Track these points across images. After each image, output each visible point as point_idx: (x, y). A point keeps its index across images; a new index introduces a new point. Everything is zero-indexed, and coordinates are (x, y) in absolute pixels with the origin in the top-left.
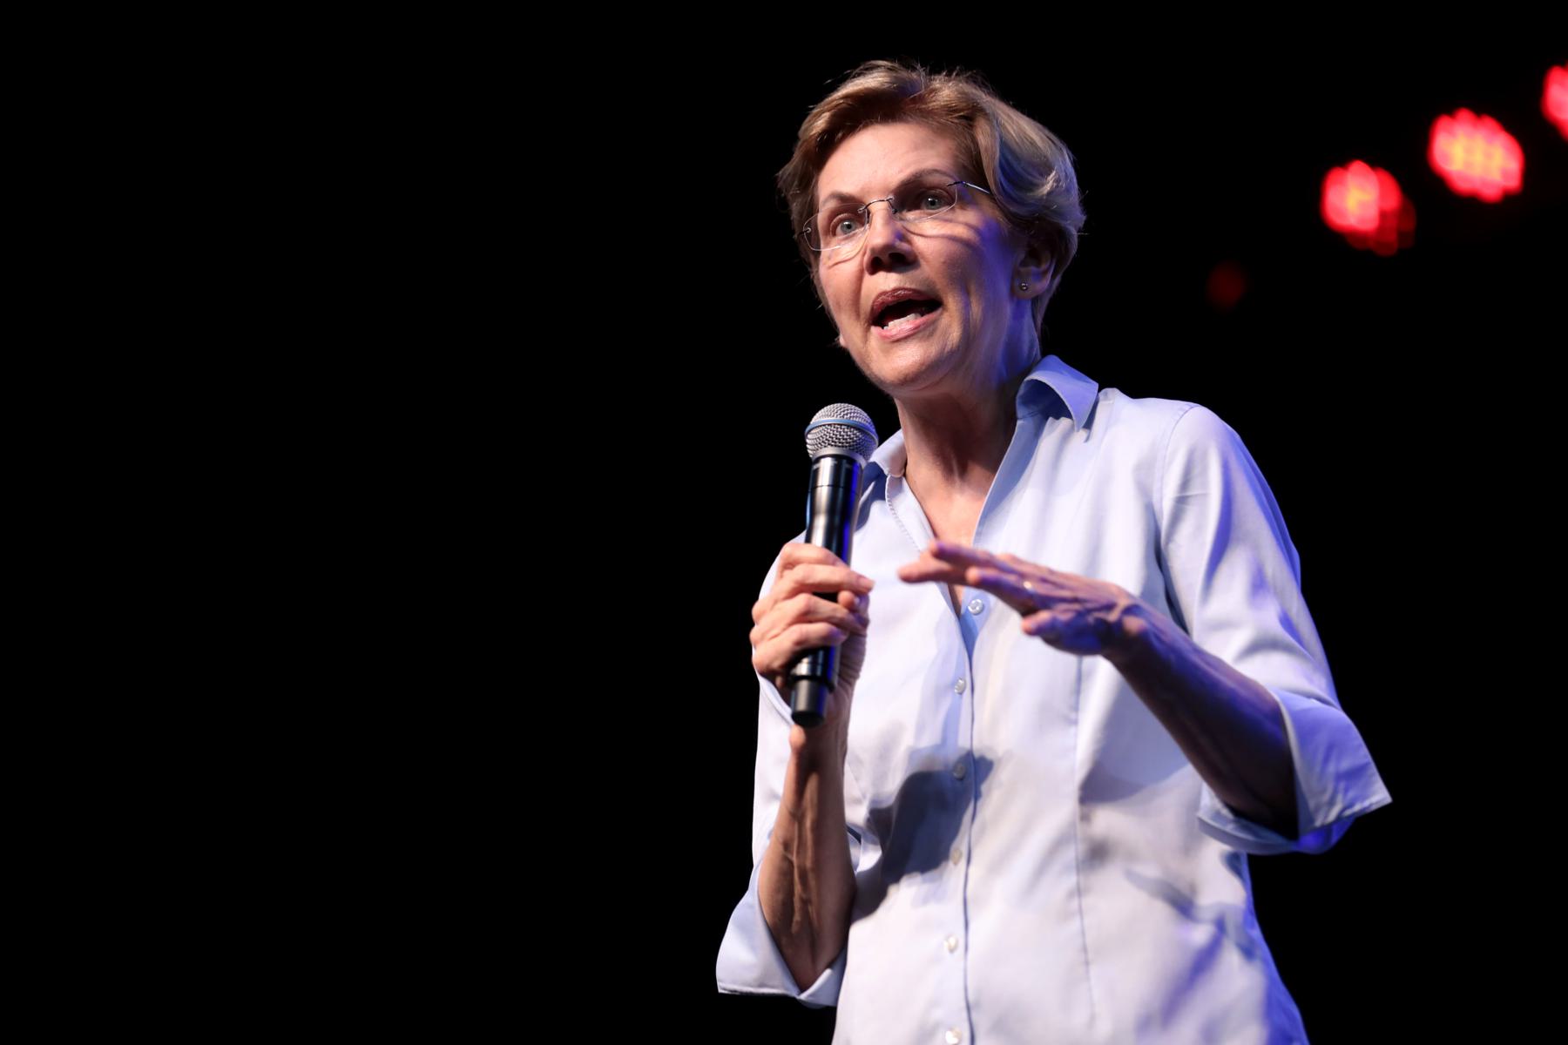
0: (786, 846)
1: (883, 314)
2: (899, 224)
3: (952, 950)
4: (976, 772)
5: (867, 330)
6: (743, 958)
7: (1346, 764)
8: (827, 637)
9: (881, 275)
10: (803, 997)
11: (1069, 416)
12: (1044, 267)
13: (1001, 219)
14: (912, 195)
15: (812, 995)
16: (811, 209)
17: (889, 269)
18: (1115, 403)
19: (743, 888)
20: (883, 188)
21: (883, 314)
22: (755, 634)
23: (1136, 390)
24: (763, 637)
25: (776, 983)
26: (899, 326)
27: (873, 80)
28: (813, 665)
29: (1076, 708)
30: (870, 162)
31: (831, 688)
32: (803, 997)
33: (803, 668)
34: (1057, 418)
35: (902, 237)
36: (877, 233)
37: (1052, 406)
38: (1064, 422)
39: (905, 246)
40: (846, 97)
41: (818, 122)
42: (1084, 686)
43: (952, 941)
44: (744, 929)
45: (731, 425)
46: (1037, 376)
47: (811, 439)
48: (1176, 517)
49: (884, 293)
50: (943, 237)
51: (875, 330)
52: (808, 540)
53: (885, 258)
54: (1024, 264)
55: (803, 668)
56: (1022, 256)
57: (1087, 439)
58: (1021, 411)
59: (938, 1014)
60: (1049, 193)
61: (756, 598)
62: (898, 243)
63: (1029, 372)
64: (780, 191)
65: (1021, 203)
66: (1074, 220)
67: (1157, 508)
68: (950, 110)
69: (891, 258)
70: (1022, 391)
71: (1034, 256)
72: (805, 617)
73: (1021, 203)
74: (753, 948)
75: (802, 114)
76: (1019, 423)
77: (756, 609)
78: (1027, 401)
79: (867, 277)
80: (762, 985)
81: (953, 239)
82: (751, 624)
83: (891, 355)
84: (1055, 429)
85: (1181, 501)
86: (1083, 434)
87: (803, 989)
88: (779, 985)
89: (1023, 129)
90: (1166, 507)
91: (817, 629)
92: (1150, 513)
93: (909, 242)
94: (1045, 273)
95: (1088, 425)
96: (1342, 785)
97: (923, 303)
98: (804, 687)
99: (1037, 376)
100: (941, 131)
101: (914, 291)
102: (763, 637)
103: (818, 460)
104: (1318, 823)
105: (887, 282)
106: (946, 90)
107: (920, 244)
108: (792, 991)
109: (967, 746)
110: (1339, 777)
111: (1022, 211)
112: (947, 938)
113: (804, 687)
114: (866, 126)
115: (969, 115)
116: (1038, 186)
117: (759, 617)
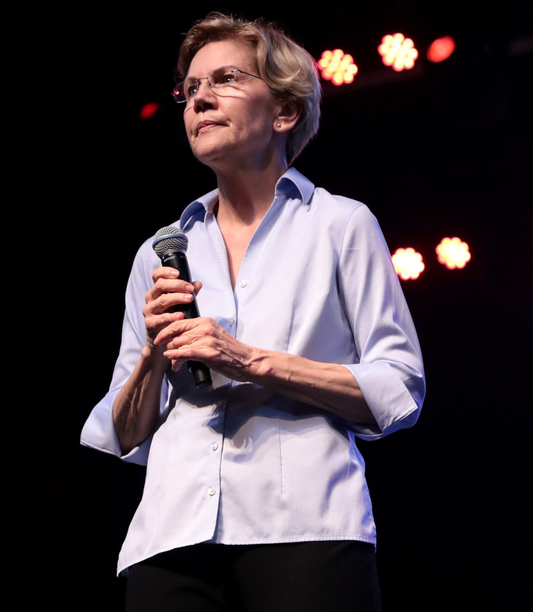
0: (130, 395)
4: (267, 73)
6: (97, 431)
7: (393, 396)
10: (123, 458)
11: (300, 198)
14: (220, 77)
18: (322, 195)
19: (102, 390)
20: (223, 81)
23: (333, 191)
25: (111, 449)
27: (215, 22)
29: (288, 342)
32: (123, 458)
34: (293, 199)
36: (201, 93)
37: (291, 191)
38: (297, 201)
39: (210, 100)
41: (189, 41)
42: (293, 331)
43: (215, 445)
44: (100, 418)
46: (286, 175)
48: (347, 260)
53: (201, 106)
54: (281, 115)
57: (308, 210)
59: (203, 479)
60: (294, 80)
67: (339, 253)
71: (286, 112)
74: (104, 430)
75: (185, 37)
76: (276, 197)
80: (103, 448)
84: (291, 204)
85: (350, 252)
86: (307, 207)
87: (124, 454)
88: (112, 450)
94: (292, 120)
95: (309, 203)
106: (250, 29)
108: (118, 454)
109: (226, 440)
112: (214, 443)
114: (204, 45)
115: (254, 41)
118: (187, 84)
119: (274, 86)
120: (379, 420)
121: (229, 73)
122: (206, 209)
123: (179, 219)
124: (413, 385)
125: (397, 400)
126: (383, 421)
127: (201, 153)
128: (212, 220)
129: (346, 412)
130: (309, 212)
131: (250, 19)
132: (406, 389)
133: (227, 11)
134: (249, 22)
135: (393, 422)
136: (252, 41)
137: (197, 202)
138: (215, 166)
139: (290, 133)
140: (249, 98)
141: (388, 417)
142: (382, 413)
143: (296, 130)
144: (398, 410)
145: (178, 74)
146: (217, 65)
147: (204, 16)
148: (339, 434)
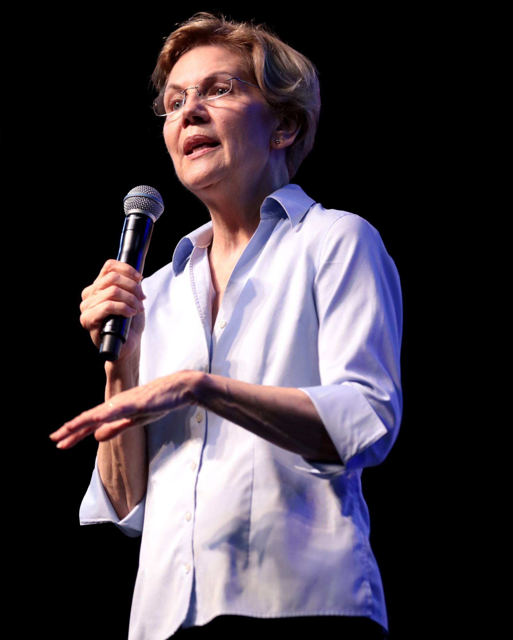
1: (190, 148)
2: (202, 101)
3: (188, 521)
7: (357, 418)
9: (190, 127)
12: (291, 132)
13: (263, 101)
14: (209, 86)
15: (125, 522)
16: (163, 81)
17: (193, 124)
21: (190, 148)
22: (82, 305)
26: (197, 153)
27: (198, 23)
28: (113, 326)
30: (192, 68)
31: (124, 341)
32: (121, 523)
33: (108, 328)
35: (201, 107)
36: (187, 107)
37: (279, 213)
38: (286, 222)
39: (203, 112)
40: (182, 31)
41: (168, 47)
43: (188, 515)
47: (126, 203)
49: (189, 138)
50: (225, 108)
51: (185, 156)
52: (119, 260)
54: (279, 129)
55: (108, 328)
56: (277, 124)
57: (298, 230)
62: (198, 111)
64: (152, 83)
65: (277, 94)
68: (240, 41)
69: (196, 118)
71: (285, 124)
72: (115, 297)
73: (277, 94)
76: (261, 221)
77: (86, 291)
78: (268, 210)
79: (183, 129)
80: (99, 517)
81: (231, 110)
82: (81, 300)
83: (190, 170)
84: (283, 224)
85: (327, 265)
87: (120, 519)
89: (295, 59)
91: (119, 305)
93: (206, 110)
95: (302, 220)
96: (356, 431)
97: (212, 143)
100: (233, 52)
101: (205, 137)
102: (87, 307)
103: (129, 215)
104: (348, 457)
106: (239, 30)
107: (211, 111)
110: (353, 427)
112: (187, 512)
114: (190, 49)
115: (248, 46)
116: (291, 86)
117: (85, 298)
119: (273, 97)
120: (340, 447)
121: (220, 85)
122: (194, 245)
123: (171, 261)
124: (382, 408)
125: (363, 423)
126: (345, 449)
127: (192, 182)
128: (202, 255)
129: (291, 429)
130: (298, 233)
131: (239, 20)
132: (372, 411)
134: (240, 22)
135: (358, 450)
137: (185, 238)
138: (203, 196)
139: (288, 150)
141: (352, 443)
142: (344, 439)
143: (293, 148)
144: (363, 434)
145: (205, 116)
146: (204, 74)
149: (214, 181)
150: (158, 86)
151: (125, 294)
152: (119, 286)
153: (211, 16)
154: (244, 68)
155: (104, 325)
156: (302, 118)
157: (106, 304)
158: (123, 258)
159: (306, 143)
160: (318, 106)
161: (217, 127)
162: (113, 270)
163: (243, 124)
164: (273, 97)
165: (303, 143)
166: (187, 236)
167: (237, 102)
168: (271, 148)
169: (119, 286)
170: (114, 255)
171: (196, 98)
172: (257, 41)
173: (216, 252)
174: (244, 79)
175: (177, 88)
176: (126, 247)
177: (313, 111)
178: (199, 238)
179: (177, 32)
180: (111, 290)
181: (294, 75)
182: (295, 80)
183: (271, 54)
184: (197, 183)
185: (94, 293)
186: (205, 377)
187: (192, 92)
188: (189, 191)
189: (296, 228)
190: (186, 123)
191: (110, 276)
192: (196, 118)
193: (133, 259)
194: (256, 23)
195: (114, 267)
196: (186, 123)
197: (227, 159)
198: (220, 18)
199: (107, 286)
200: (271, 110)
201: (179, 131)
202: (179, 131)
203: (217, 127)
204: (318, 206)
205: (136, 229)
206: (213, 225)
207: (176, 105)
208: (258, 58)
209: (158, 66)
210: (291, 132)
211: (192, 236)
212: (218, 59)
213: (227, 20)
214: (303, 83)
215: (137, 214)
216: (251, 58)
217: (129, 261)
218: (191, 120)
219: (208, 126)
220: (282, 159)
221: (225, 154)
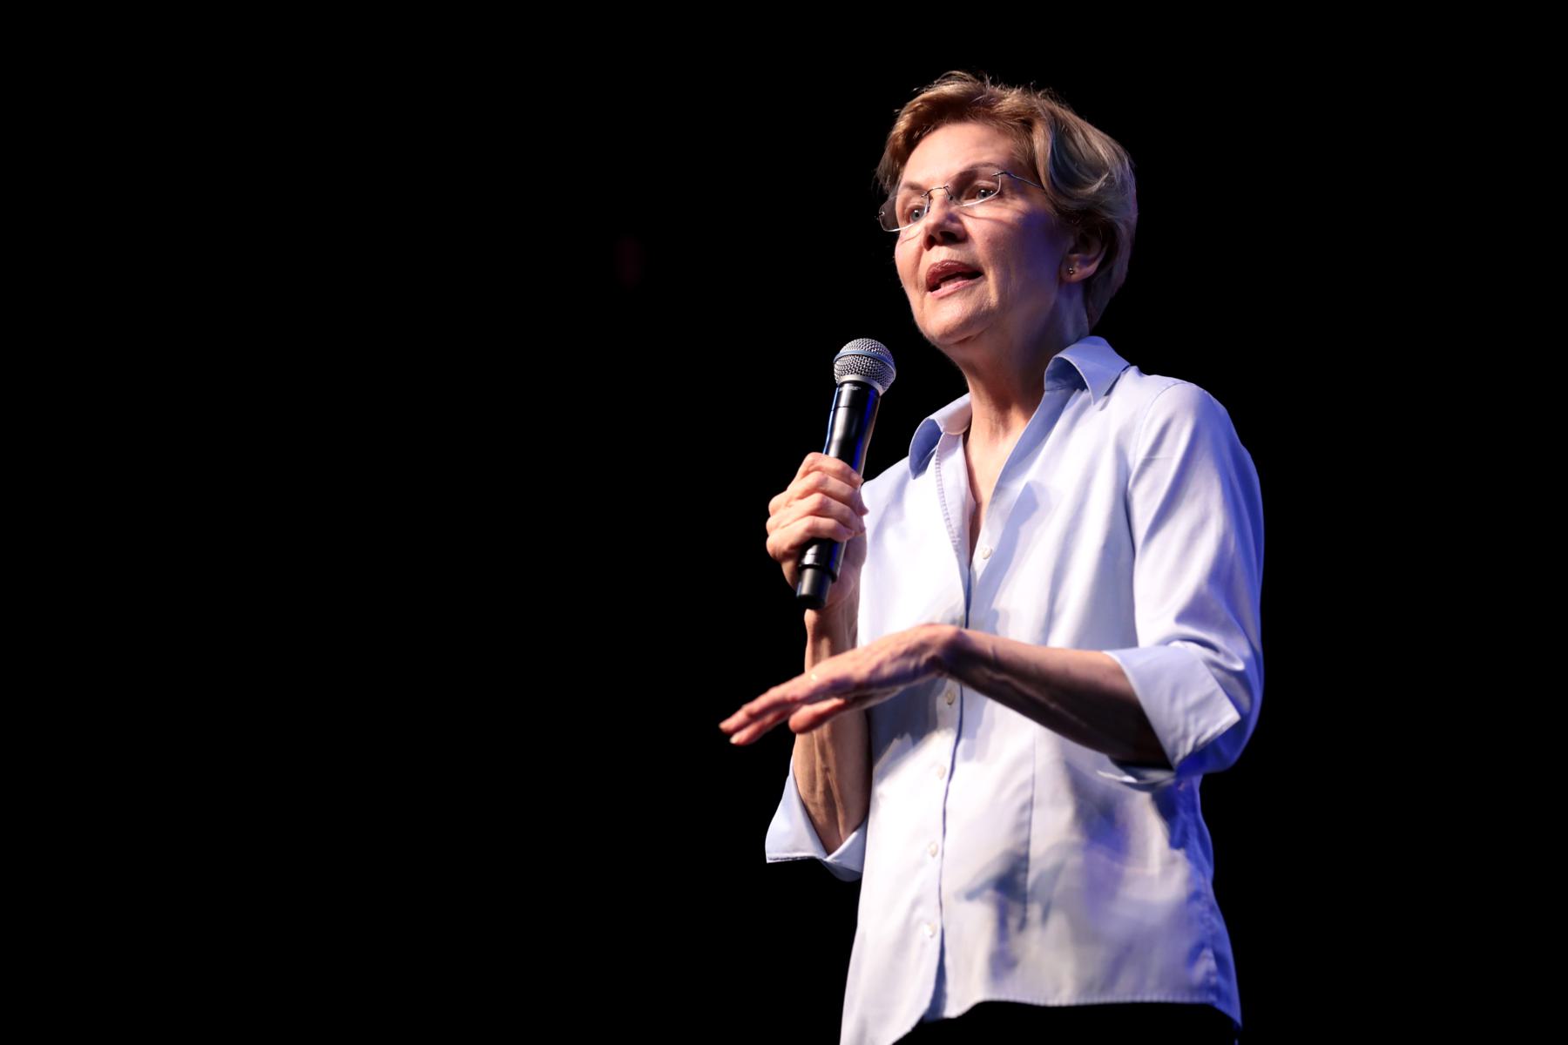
1: (935, 282)
2: (954, 208)
5: (923, 297)
7: (1193, 697)
8: (834, 531)
9: (935, 248)
12: (1092, 256)
13: (1049, 208)
14: (965, 186)
16: (895, 178)
17: (941, 244)
21: (935, 282)
22: (770, 523)
23: (1146, 369)
24: (776, 527)
27: (948, 88)
28: (818, 556)
30: (940, 157)
31: (834, 578)
33: (809, 558)
35: (953, 218)
36: (931, 218)
37: (1073, 381)
38: (1085, 395)
39: (956, 226)
40: (924, 101)
41: (902, 125)
45: (796, 342)
46: (1063, 355)
54: (1073, 251)
55: (809, 558)
56: (1071, 244)
57: (1102, 408)
58: (1047, 385)
60: (1100, 190)
61: (784, 489)
63: (1061, 348)
65: (1070, 198)
66: (1126, 214)
68: (1014, 115)
69: (946, 234)
70: (1050, 367)
71: (1083, 244)
72: (819, 511)
73: (1070, 198)
78: (1055, 376)
81: (998, 221)
82: (766, 535)
83: (937, 314)
84: (1080, 398)
89: (1097, 144)
90: (1136, 456)
91: (826, 523)
92: (1121, 454)
93: (960, 222)
94: (1094, 260)
97: (971, 273)
98: (808, 574)
99: (1063, 355)
100: (1003, 132)
103: (842, 385)
105: (941, 254)
106: (1011, 99)
107: (969, 224)
111: (1072, 205)
113: (808, 574)
114: (935, 128)
115: (1026, 124)
118: (901, 198)
119: (1063, 202)
120: (1167, 741)
124: (1232, 682)
125: (1202, 704)
126: (1175, 746)
131: (1011, 83)
132: (1216, 686)
133: (976, 67)
135: (1195, 746)
136: (1022, 121)
138: (956, 355)
139: (1087, 283)
140: (1018, 216)
146: (957, 166)
147: (927, 82)
148: (1001, 578)
149: (973, 332)
150: (887, 186)
151: (836, 506)
152: (827, 493)
153: (968, 77)
154: (1019, 157)
155: (803, 554)
156: (1108, 234)
157: (807, 522)
158: (833, 450)
159: (1115, 273)
160: (1132, 215)
161: (979, 248)
162: (818, 469)
163: (1018, 244)
164: (1063, 202)
165: (1110, 274)
166: (932, 417)
167: (1009, 210)
168: (1061, 281)
169: (827, 493)
170: (820, 446)
171: (945, 204)
172: (1039, 115)
173: (976, 441)
174: (1019, 175)
175: (916, 189)
176: (838, 433)
177: (1126, 223)
178: (950, 420)
179: (917, 102)
180: (815, 499)
181: (1097, 169)
182: (1098, 176)
183: (1061, 136)
184: (947, 334)
185: (788, 504)
186: (960, 634)
187: (939, 194)
188: (934, 348)
189: (1100, 404)
190: (930, 242)
191: (812, 479)
192: (946, 234)
193: (848, 452)
194: (1037, 89)
195: (818, 464)
196: (930, 242)
197: (993, 298)
198: (982, 80)
199: (808, 493)
200: (1061, 223)
201: (920, 255)
202: (920, 255)
203: (979, 248)
204: (1133, 370)
205: (853, 406)
206: (972, 400)
207: (914, 214)
208: (1041, 141)
209: (887, 155)
210: (1092, 256)
211: (939, 416)
212: (980, 144)
213: (994, 83)
214: (1110, 181)
215: (854, 383)
216: (1030, 141)
217: (842, 455)
218: (938, 237)
219: (965, 246)
220: (1078, 298)
221: (990, 289)
